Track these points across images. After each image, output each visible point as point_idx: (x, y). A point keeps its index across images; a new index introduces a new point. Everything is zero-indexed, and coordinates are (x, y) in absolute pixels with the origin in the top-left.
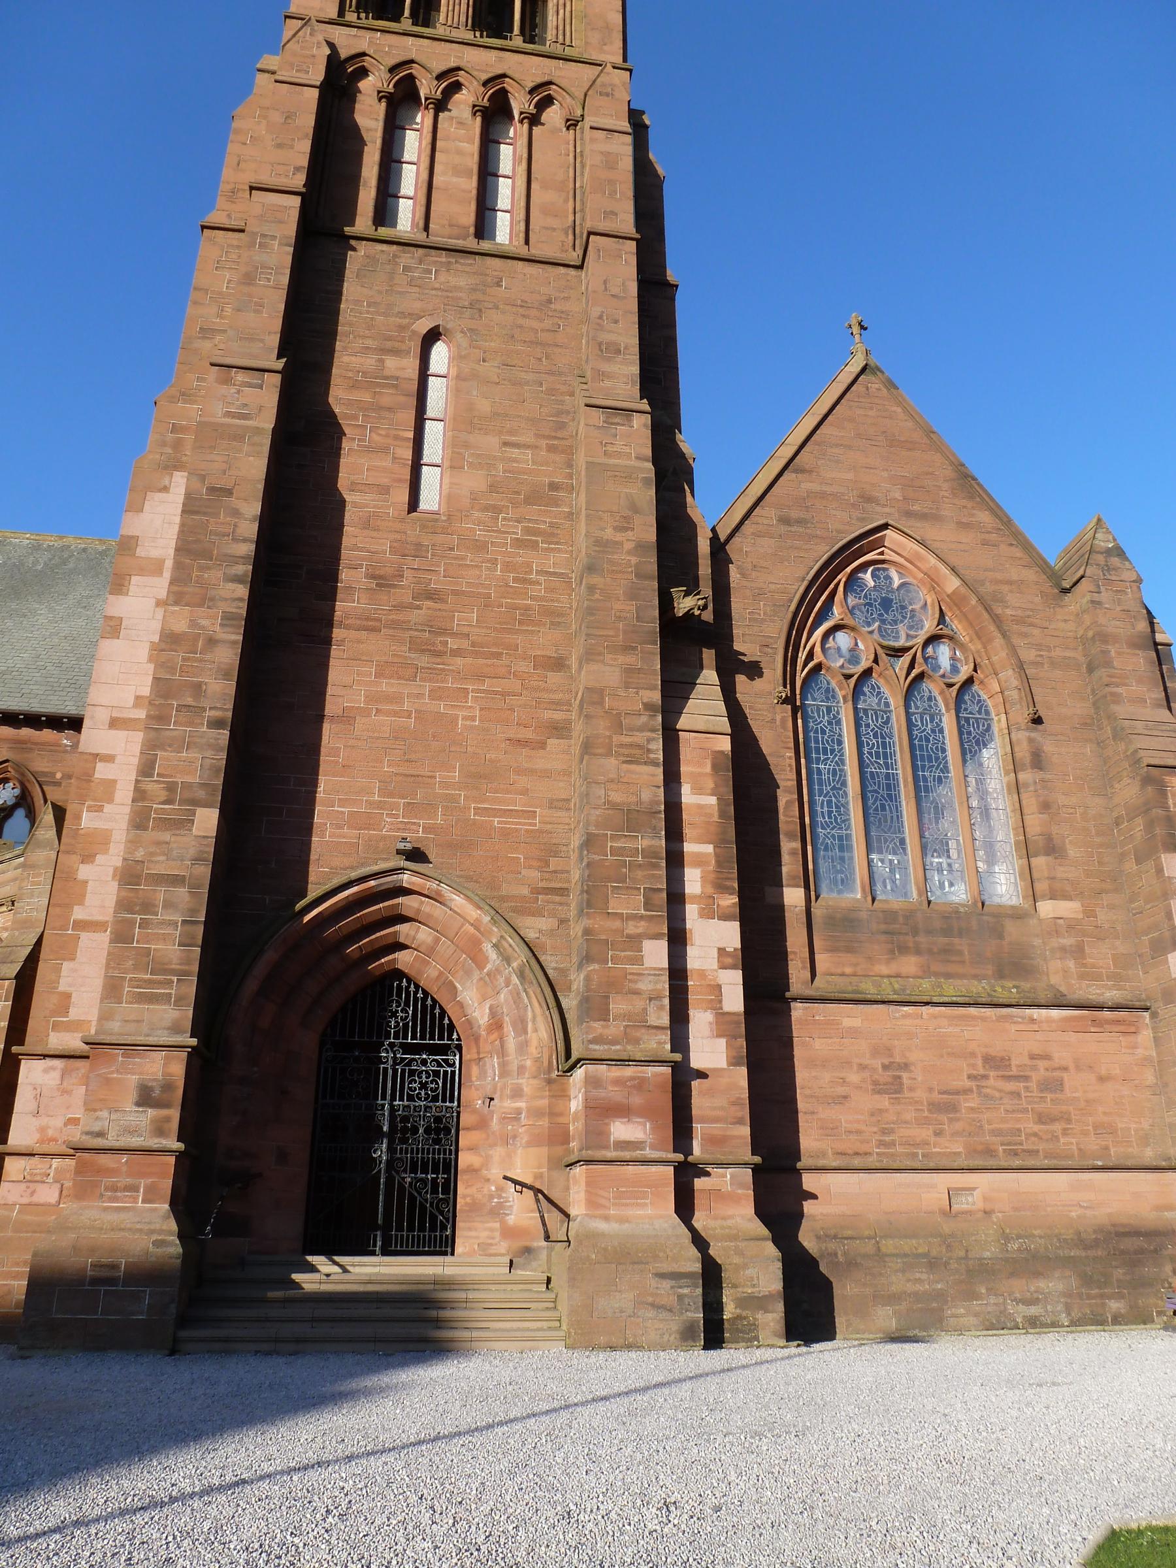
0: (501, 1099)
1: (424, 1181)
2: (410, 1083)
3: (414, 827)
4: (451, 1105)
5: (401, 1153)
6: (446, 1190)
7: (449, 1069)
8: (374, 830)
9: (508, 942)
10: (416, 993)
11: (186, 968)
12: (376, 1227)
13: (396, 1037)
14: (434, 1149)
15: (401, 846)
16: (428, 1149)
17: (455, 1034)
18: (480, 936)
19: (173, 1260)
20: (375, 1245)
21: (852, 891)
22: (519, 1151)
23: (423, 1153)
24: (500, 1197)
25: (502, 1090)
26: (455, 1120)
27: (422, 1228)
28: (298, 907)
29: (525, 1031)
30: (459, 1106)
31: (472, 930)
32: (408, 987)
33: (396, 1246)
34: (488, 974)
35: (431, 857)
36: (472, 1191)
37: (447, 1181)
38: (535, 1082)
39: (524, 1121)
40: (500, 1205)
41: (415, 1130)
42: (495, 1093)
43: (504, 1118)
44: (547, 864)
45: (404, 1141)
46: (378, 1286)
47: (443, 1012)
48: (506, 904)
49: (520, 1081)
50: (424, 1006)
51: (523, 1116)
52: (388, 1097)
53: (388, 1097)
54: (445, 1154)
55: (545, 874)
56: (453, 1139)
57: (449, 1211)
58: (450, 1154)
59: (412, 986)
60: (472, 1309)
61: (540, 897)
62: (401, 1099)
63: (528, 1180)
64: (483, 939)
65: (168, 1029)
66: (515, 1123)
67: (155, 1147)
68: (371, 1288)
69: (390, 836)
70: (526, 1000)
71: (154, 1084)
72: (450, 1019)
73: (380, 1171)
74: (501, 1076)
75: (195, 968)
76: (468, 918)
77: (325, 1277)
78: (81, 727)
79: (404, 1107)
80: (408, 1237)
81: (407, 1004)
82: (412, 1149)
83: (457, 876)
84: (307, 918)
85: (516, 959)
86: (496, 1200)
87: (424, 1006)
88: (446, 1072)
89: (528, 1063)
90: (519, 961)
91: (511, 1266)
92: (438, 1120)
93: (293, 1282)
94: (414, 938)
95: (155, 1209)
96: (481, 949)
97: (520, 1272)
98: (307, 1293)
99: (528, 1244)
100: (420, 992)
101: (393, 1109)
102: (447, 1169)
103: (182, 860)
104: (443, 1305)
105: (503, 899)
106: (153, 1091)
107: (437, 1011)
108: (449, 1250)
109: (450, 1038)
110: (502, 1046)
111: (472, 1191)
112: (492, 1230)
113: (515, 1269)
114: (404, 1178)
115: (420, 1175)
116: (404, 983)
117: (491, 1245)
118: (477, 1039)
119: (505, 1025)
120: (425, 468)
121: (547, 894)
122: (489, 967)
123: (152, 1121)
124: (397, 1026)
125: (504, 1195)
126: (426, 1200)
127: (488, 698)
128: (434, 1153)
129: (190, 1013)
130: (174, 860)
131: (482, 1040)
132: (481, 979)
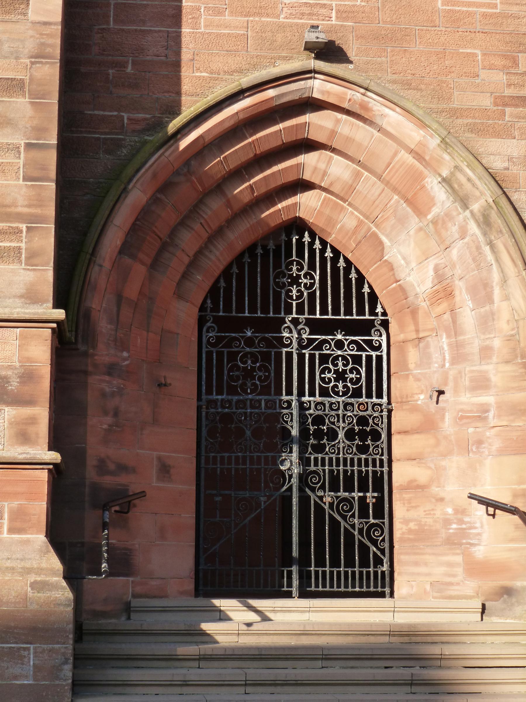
0: (456, 391)
1: (348, 501)
2: (322, 372)
3: (323, 11)
4: (378, 401)
5: (316, 465)
6: (379, 513)
7: (374, 354)
8: (268, 15)
9: (465, 175)
10: (323, 251)
11: (38, 211)
12: (288, 561)
13: (300, 311)
14: (359, 460)
15: (312, 37)
16: (352, 460)
17: (379, 306)
18: (421, 168)
19: (62, 608)
20: (290, 585)
22: (488, 462)
23: (345, 465)
24: (461, 522)
25: (456, 380)
26: (385, 420)
27: (350, 563)
28: (173, 125)
29: (489, 299)
30: (389, 403)
31: (410, 159)
32: (311, 244)
33: (317, 586)
34: (435, 222)
35: (351, 54)
36: (418, 513)
37: (380, 501)
38: (508, 368)
39: (492, 422)
40: (463, 533)
41: (333, 435)
42: (446, 384)
43: (462, 418)
44: (515, 63)
45: (319, 448)
46: (315, 637)
47: (361, 279)
48: (459, 121)
49: (484, 368)
50: (335, 270)
51: (491, 414)
52: (295, 391)
53: (295, 391)
54: (374, 466)
55: (513, 77)
56: (385, 446)
57: (383, 540)
58: (382, 466)
59: (317, 242)
60: (449, 668)
61: (508, 110)
62: (312, 394)
63: (505, 498)
64: (426, 172)
65: (21, 296)
66: (479, 424)
67: (21, 458)
68: (305, 641)
69: (291, 26)
70: (490, 257)
71: (10, 373)
72: (370, 287)
73: (290, 489)
74: (455, 361)
75: (51, 211)
76: (408, 142)
77: (245, 627)
79: (317, 404)
80: (332, 573)
81: (312, 266)
82: (331, 459)
83: (390, 82)
84: (184, 143)
85: (477, 199)
86: (454, 526)
87: (335, 270)
88: (369, 358)
89: (497, 343)
90: (482, 202)
91: (483, 612)
92: (363, 421)
93: (204, 634)
94: (325, 173)
95: (27, 542)
96: (423, 187)
97: (495, 619)
98: (225, 649)
99: (507, 583)
101: (302, 407)
102: (378, 486)
103: (17, 58)
104: (443, 663)
105: (455, 113)
106: (8, 382)
107: (353, 275)
108: (387, 590)
109: (373, 312)
110: (454, 322)
111: (418, 513)
112: (450, 565)
113: (490, 615)
114: (321, 498)
115: (343, 494)
116: (307, 238)
117: (451, 584)
118: (414, 312)
119: (457, 293)
121: (516, 106)
122: (435, 211)
123: (11, 423)
124: (300, 295)
125: (467, 519)
126: (353, 526)
128: (360, 465)
129: (49, 275)
130: (6, 57)
131: (421, 313)
132: (421, 229)
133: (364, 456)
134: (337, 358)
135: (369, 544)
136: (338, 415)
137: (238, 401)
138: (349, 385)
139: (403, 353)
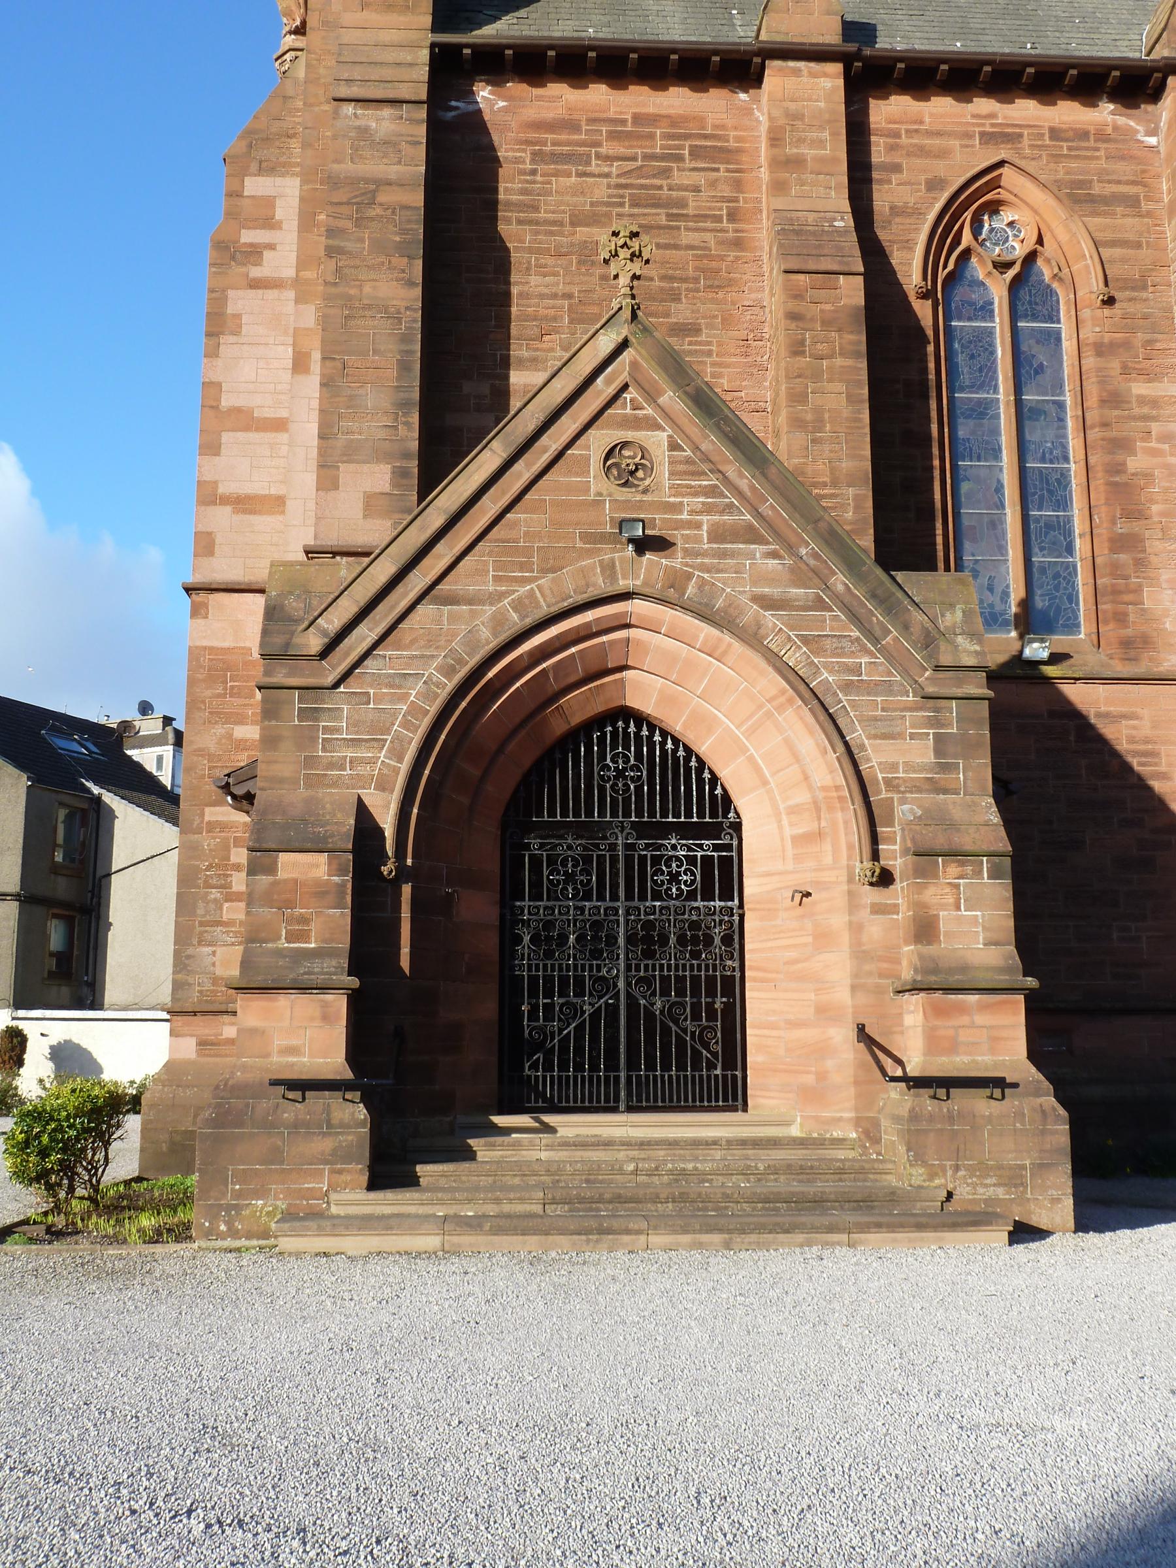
21: (1080, 633)
47: (714, 779)
59: (669, 741)
78: (1100, 1228)
82: (560, 965)
100: (681, 748)
120: (424, 97)
126: (685, 1031)
127: (810, 100)
133: (650, 962)
134: (670, 858)
135: (700, 1048)
136: (715, 921)
137: (662, 908)
138: (683, 887)
139: (972, 863)
